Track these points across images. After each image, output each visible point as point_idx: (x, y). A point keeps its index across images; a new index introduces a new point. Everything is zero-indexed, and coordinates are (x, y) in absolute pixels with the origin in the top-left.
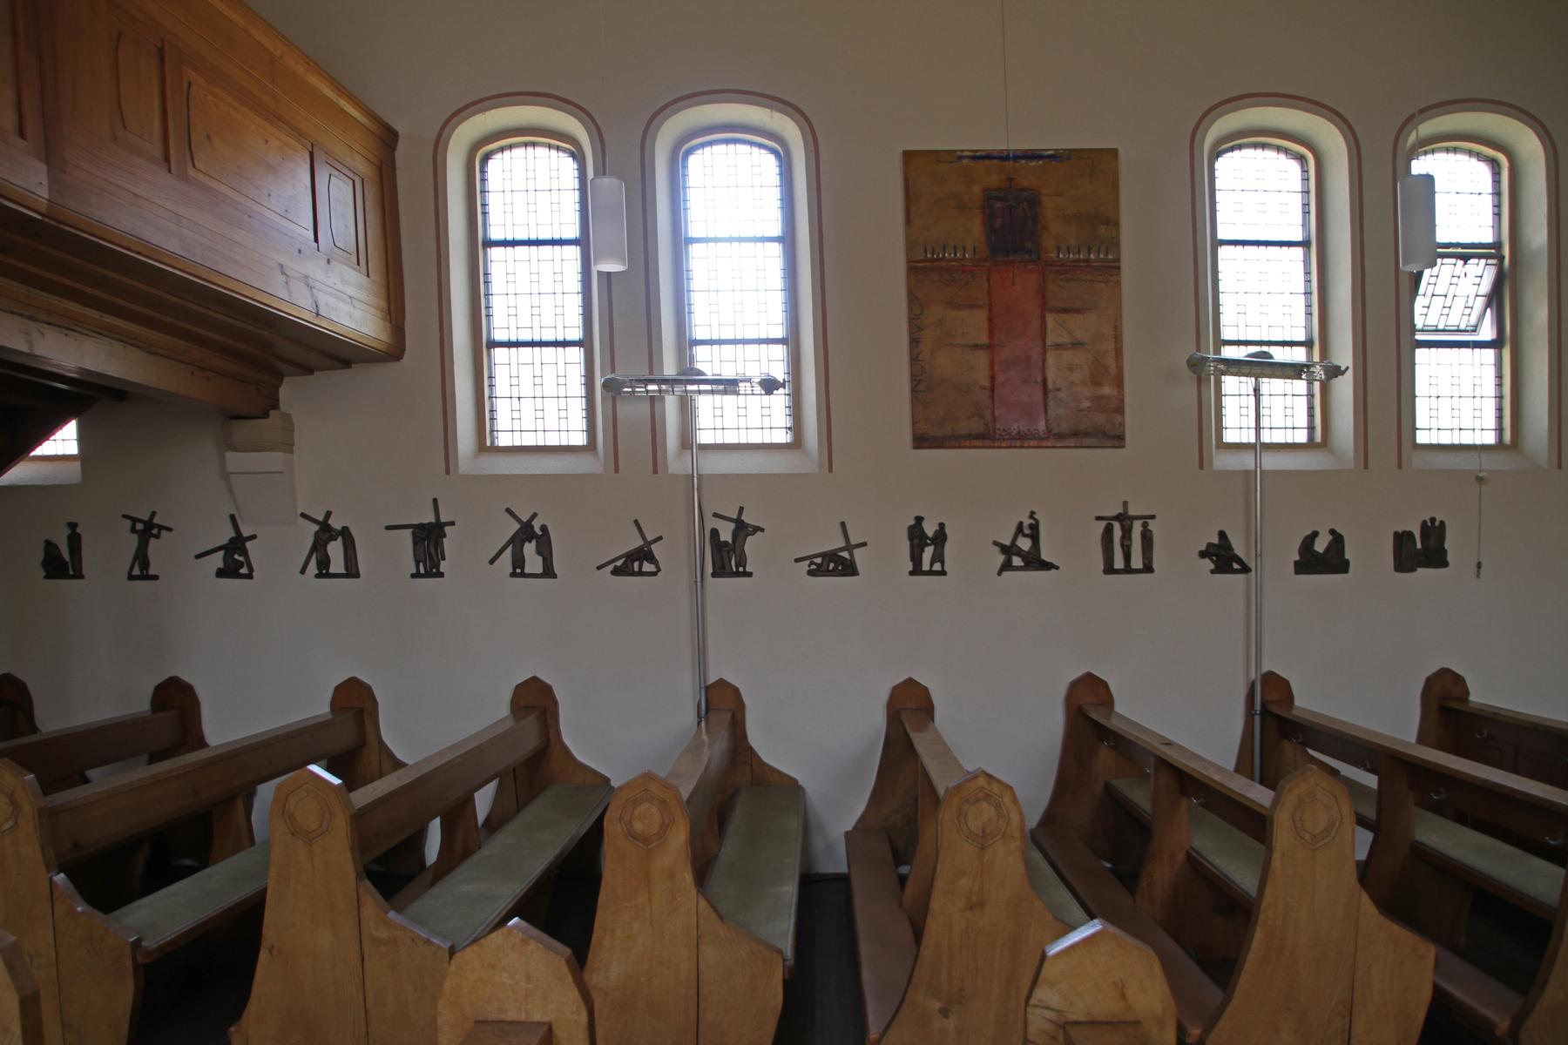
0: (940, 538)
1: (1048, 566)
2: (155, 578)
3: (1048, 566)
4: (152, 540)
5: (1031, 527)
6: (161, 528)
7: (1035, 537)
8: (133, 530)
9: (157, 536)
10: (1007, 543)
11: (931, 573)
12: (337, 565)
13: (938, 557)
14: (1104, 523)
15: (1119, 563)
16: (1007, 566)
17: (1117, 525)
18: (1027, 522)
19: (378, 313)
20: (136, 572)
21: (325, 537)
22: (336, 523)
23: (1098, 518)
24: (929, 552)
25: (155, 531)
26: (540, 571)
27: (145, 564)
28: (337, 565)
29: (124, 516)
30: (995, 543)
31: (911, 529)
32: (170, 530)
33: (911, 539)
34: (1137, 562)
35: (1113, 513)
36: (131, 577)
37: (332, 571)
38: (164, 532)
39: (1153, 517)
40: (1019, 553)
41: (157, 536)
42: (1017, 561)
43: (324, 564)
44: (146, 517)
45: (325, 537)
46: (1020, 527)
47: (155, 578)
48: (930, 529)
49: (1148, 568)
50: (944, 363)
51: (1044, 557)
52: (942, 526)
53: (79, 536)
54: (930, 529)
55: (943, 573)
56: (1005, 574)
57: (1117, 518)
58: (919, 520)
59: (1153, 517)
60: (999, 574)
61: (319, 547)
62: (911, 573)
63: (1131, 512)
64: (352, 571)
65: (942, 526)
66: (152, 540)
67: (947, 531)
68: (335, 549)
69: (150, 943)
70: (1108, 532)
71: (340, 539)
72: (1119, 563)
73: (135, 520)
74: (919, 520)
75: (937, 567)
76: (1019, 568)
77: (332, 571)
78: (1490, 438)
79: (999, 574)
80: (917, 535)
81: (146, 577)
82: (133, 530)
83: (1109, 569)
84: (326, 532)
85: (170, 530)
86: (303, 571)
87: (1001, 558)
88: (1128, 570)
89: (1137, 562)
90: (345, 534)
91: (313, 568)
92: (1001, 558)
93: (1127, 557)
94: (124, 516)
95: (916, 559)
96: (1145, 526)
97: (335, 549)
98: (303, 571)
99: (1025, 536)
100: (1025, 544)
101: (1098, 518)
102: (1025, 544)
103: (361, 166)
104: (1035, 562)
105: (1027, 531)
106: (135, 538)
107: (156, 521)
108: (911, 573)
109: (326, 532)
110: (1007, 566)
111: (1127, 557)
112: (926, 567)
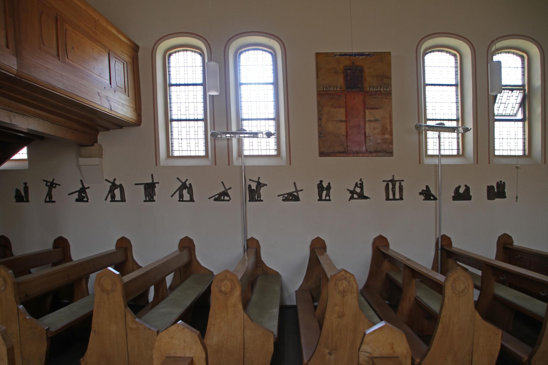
0: (329, 188)
1: (366, 198)
2: (54, 202)
3: (366, 198)
4: (53, 189)
5: (360, 184)
6: (56, 184)
7: (362, 188)
8: (47, 185)
9: (55, 187)
10: (352, 190)
11: (325, 200)
12: (118, 198)
13: (328, 195)
14: (386, 183)
15: (391, 197)
16: (352, 198)
17: (390, 183)
18: (359, 182)
19: (132, 109)
20: (48, 200)
21: (114, 187)
22: (117, 183)
23: (384, 181)
24: (325, 193)
25: (54, 186)
26: (189, 199)
27: (51, 197)
28: (118, 198)
29: (43, 180)
30: (348, 190)
31: (318, 185)
32: (59, 185)
33: (318, 188)
34: (397, 196)
35: (389, 179)
36: (46, 202)
37: (116, 199)
38: (57, 186)
39: (403, 181)
40: (356, 193)
41: (55, 187)
42: (355, 196)
43: (113, 197)
44: (51, 181)
45: (114, 187)
46: (356, 184)
47: (54, 202)
48: (325, 185)
49: (401, 198)
50: (330, 127)
51: (365, 194)
52: (329, 184)
53: (28, 187)
54: (325, 185)
55: (329, 200)
56: (351, 200)
57: (390, 181)
58: (321, 181)
59: (403, 181)
60: (349, 200)
61: (111, 191)
62: (318, 200)
63: (395, 179)
64: (123, 200)
65: (329, 184)
66: (53, 189)
67: (331, 185)
68: (117, 192)
69: (52, 329)
70: (387, 186)
71: (119, 188)
72: (391, 197)
73: (47, 182)
74: (321, 181)
75: (327, 198)
76: (356, 199)
77: (116, 199)
78: (521, 153)
79: (349, 200)
80: (320, 187)
81: (51, 201)
82: (47, 185)
83: (388, 199)
84: (114, 186)
85: (59, 185)
86: (106, 200)
87: (350, 195)
88: (394, 199)
89: (397, 196)
90: (121, 186)
91: (109, 198)
92: (350, 195)
93: (394, 195)
94: (43, 180)
95: (320, 195)
96: (400, 184)
97: (117, 192)
98: (106, 200)
99: (358, 187)
100: (358, 190)
101: (384, 181)
102: (358, 190)
103: (126, 58)
104: (362, 196)
105: (359, 186)
106: (47, 188)
107: (54, 182)
108: (318, 200)
109: (114, 186)
110: (352, 198)
111: (394, 195)
112: (324, 198)
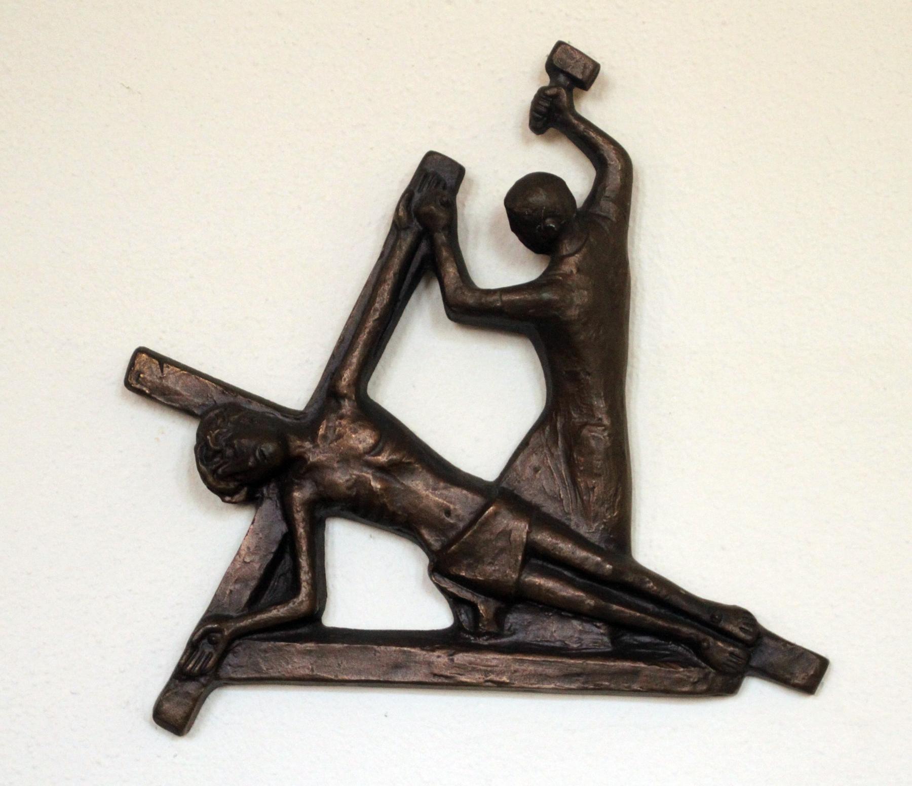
1: (701, 648)
3: (701, 648)
5: (535, 212)
7: (574, 303)
10: (284, 373)
16: (262, 630)
18: (499, 157)
30: (152, 379)
40: (396, 482)
42: (376, 580)
46: (422, 231)
50: (166, 706)
51: (683, 536)
53: (725, 684)
56: (236, 711)
60: (176, 711)
69: (515, 492)
76: (386, 659)
79: (176, 711)
87: (217, 538)
92: (217, 538)
99: (476, 312)
100: (468, 399)
102: (468, 399)
104: (568, 591)
105: (497, 263)
110: (262, 630)
